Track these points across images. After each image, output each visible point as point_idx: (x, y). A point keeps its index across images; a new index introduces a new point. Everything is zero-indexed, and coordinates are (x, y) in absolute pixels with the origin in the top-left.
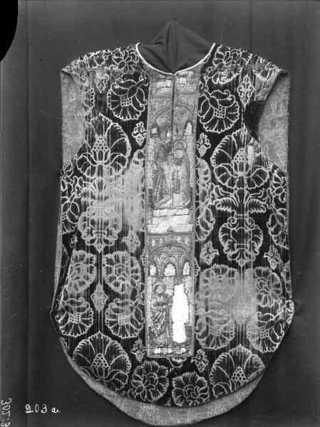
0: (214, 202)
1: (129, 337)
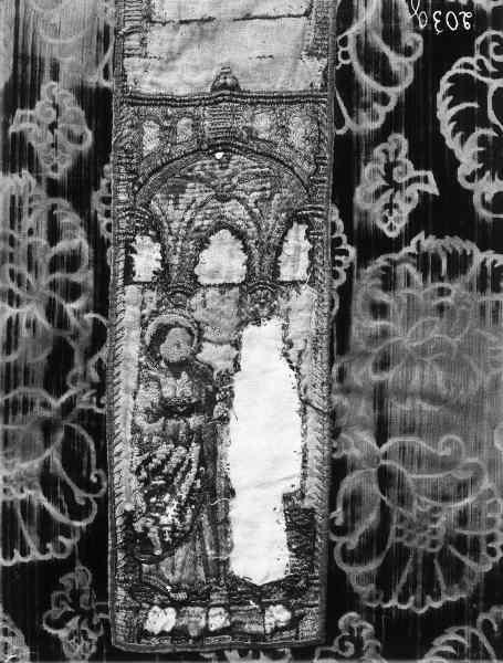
1: (35, 555)
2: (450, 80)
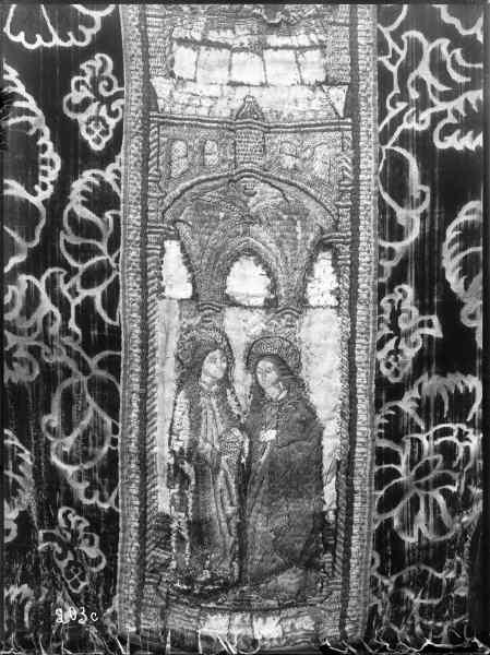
0: (426, 115)
1: (57, 41)
2: (456, 229)
